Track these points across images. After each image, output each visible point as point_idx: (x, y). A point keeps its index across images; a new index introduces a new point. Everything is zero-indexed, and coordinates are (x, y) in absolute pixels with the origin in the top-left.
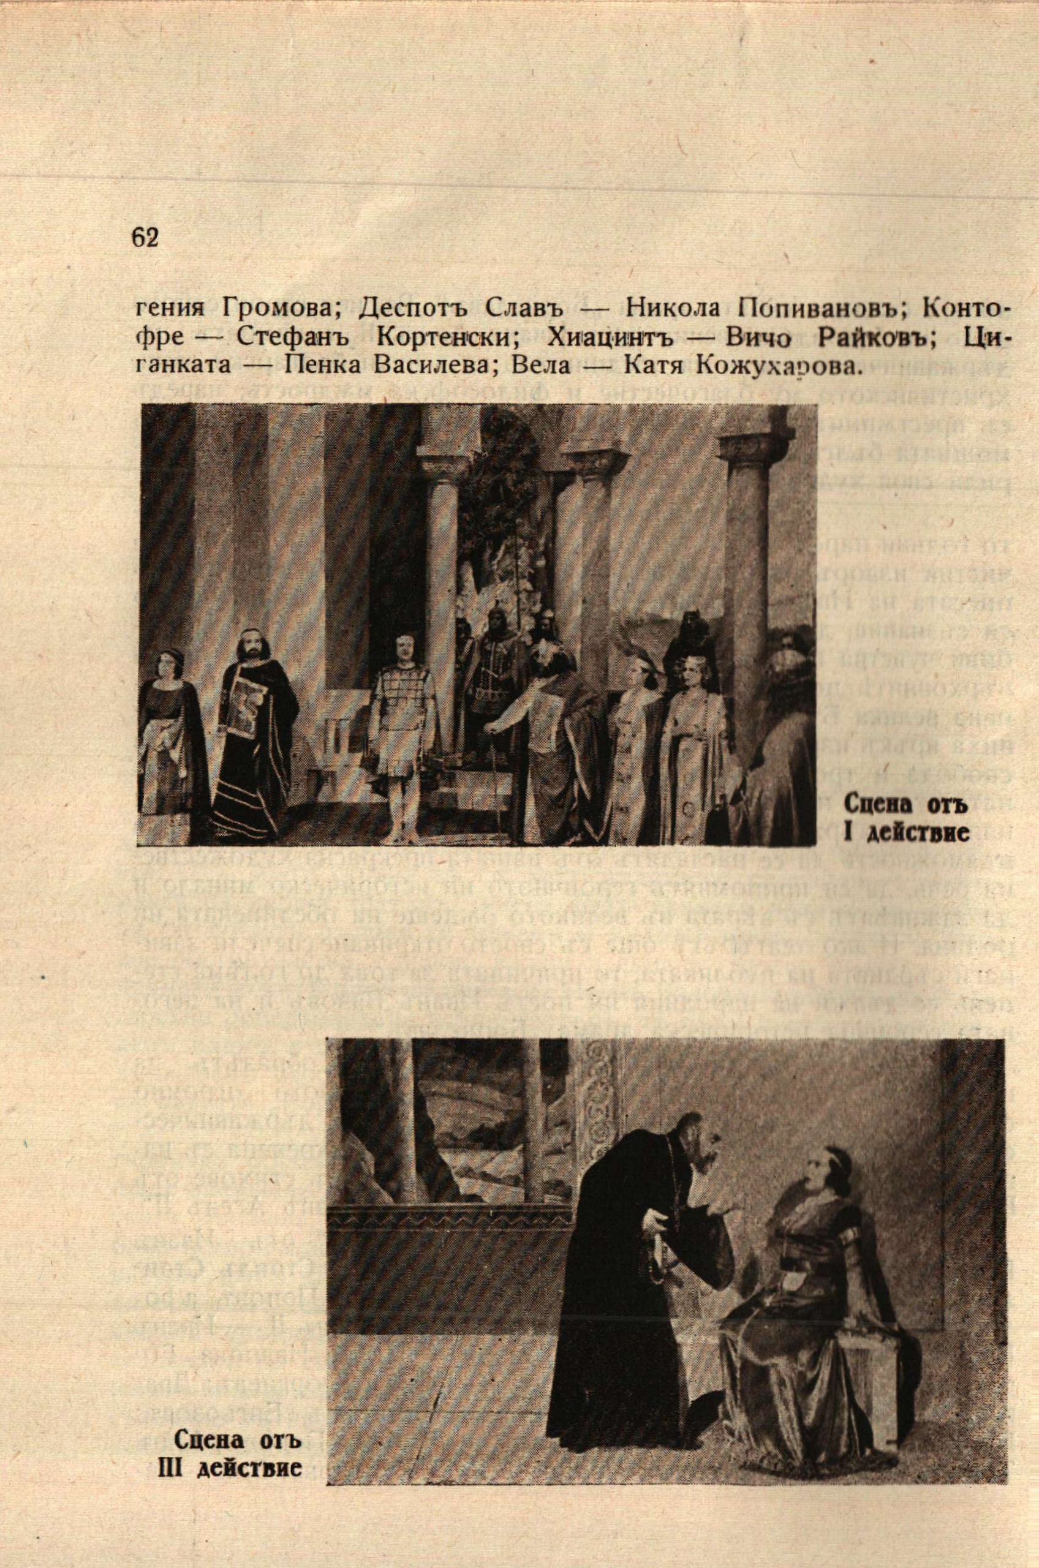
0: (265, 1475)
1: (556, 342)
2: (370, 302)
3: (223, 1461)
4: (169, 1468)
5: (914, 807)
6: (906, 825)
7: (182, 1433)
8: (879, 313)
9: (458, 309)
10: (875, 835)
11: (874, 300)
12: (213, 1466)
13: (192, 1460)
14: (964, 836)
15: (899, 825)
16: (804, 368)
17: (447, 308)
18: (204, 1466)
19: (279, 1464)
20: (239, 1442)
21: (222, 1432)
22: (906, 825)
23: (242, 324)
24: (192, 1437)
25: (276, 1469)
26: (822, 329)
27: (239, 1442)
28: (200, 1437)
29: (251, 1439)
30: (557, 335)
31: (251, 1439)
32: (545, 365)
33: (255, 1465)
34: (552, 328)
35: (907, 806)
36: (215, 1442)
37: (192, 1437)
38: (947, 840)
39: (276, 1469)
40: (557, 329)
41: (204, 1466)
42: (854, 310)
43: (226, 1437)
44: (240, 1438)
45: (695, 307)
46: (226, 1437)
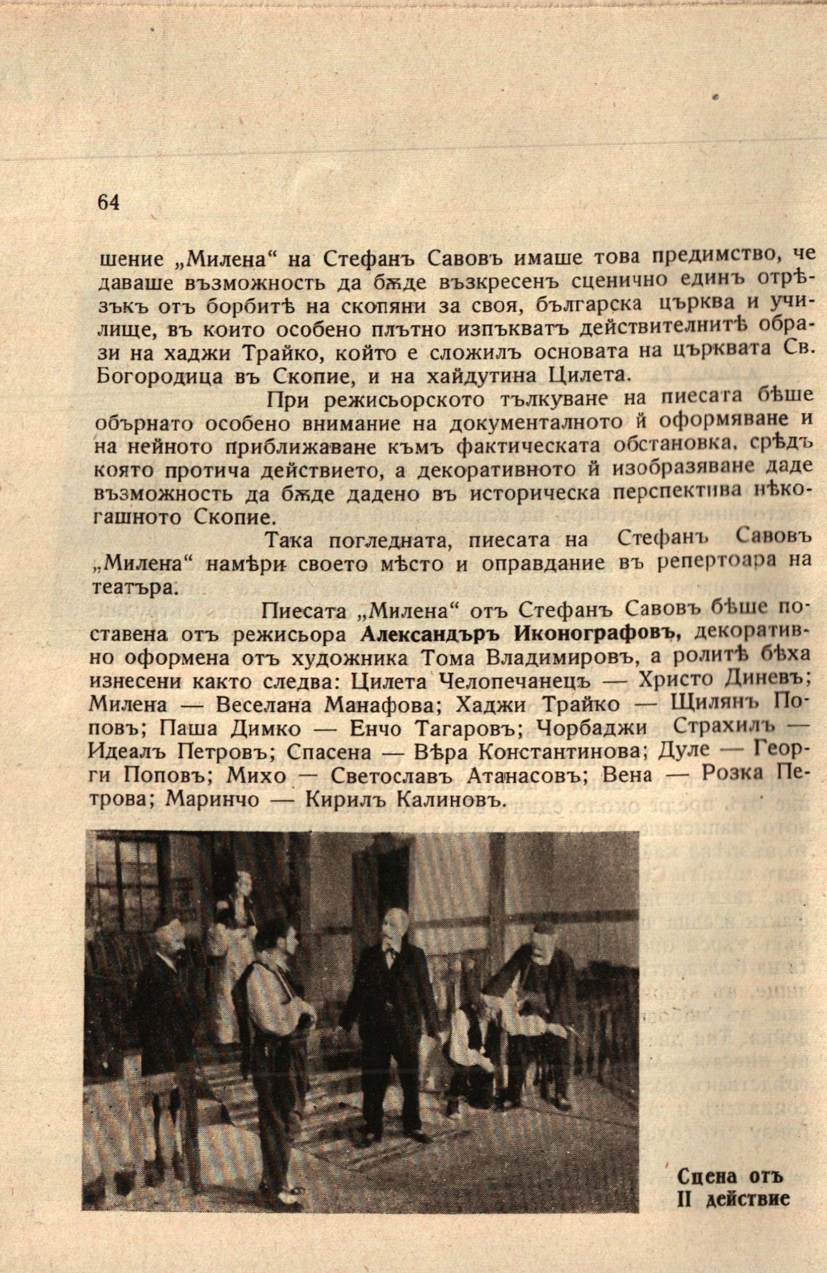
0: (760, 1204)
1: (463, 709)
2: (240, 724)
3: (726, 1194)
4: (684, 1199)
5: (738, 1179)
6: (738, 1194)
7: (684, 1172)
8: (659, 635)
9: (517, 400)
10: (712, 1202)
11: (681, 602)
12: (719, 1199)
13: (700, 1193)
14: (786, 1201)
15: (732, 1193)
16: (759, 560)
17: (130, 376)
18: (711, 1198)
19: (771, 1195)
20: (733, 1179)
21: (721, 1170)
22: (738, 1194)
23: (787, 337)
24: (694, 1175)
25: (768, 1199)
26: (219, 698)
27: (733, 1179)
28: (653, 637)
29: (743, 1175)
30: (463, 704)
31: (743, 1175)
32: (404, 776)
33: (751, 1197)
34: (460, 698)
35: (733, 1178)
36: (715, 1178)
37: (694, 1175)
38: (771, 1204)
39: (768, 1199)
40: (464, 699)
41: (711, 1198)
42: (588, 422)
43: (724, 1174)
44: (734, 1175)
45: (700, 654)
46: (724, 1174)
